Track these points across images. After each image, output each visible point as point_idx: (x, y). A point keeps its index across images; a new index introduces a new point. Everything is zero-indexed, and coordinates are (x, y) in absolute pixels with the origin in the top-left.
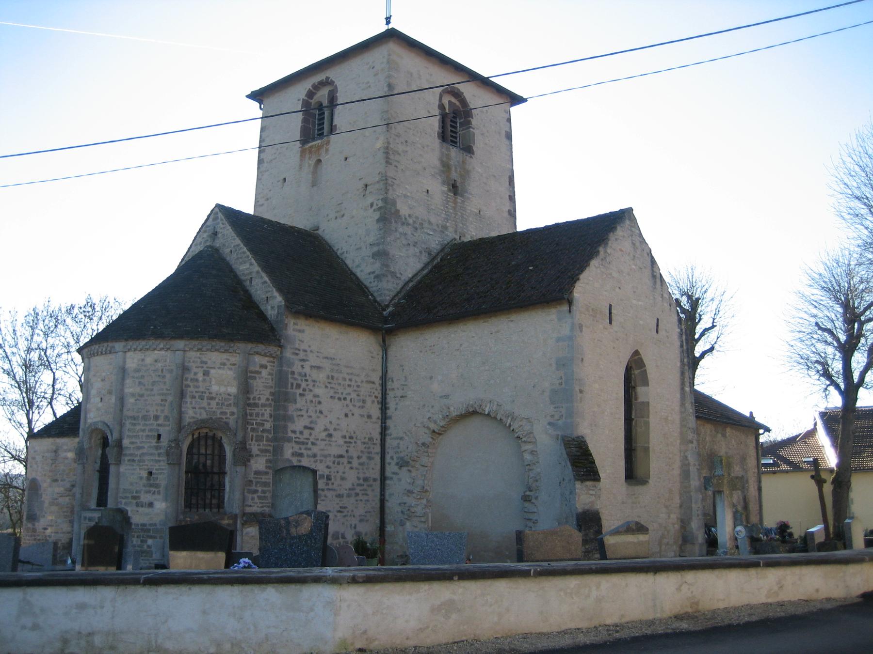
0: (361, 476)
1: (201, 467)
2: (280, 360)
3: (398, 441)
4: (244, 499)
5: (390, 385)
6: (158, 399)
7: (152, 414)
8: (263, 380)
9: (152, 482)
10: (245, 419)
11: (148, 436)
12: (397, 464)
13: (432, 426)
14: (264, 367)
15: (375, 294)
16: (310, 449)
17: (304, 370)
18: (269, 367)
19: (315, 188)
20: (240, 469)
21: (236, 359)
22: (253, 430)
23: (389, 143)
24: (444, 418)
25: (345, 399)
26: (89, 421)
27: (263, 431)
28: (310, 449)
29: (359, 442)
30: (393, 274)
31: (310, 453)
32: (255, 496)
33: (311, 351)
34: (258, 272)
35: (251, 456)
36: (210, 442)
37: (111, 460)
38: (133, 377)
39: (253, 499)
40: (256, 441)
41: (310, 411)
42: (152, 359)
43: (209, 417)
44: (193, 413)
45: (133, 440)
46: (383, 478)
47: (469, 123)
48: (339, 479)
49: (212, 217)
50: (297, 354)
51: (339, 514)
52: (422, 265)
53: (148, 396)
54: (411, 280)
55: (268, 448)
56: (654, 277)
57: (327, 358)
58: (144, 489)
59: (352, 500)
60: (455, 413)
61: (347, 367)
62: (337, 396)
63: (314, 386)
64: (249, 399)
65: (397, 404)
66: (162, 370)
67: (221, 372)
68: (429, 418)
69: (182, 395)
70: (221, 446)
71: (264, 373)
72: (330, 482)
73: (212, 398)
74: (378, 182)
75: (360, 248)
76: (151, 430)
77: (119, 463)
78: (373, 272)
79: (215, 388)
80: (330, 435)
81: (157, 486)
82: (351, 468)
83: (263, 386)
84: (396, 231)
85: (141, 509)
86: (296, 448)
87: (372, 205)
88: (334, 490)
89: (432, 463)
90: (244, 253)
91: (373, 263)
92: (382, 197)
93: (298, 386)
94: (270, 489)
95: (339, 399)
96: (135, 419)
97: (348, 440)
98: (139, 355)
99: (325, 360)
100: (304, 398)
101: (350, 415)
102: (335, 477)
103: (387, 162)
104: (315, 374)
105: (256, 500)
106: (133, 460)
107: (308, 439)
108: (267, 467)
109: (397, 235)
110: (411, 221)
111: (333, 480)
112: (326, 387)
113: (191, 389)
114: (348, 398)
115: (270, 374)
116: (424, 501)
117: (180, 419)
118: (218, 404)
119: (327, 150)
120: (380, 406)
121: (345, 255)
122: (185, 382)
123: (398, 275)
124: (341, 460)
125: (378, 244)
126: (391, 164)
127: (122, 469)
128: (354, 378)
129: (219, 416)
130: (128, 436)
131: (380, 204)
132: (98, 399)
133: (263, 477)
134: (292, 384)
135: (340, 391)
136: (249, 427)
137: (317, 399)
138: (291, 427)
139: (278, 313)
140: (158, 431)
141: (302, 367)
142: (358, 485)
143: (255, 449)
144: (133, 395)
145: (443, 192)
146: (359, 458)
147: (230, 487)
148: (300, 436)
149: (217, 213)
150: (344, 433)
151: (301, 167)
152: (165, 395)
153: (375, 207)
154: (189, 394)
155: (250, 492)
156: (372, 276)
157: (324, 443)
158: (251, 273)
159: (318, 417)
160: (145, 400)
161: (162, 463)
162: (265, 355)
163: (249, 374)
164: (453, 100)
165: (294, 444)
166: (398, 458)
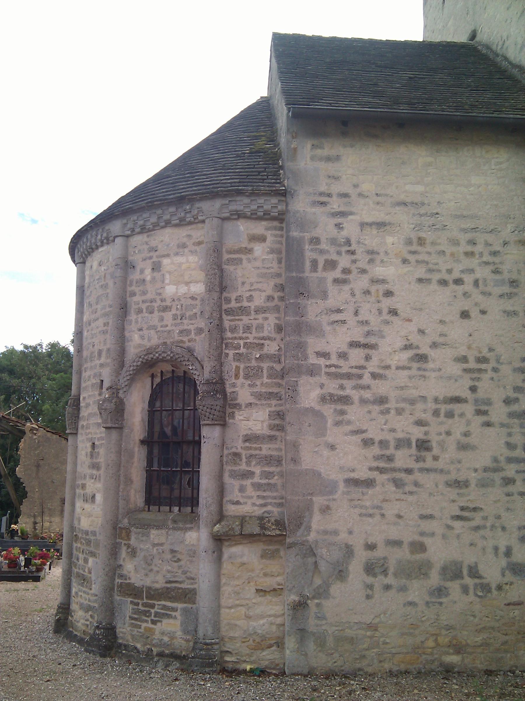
14: (262, 239)
17: (344, 233)
18: (270, 239)
21: (198, 233)
22: (238, 357)
25: (458, 282)
27: (261, 359)
28: (368, 387)
29: (506, 370)
32: (248, 483)
33: (360, 195)
37: (260, 456)
39: (242, 489)
51: (457, 524)
59: (496, 492)
62: (436, 277)
67: (179, 259)
69: (124, 309)
71: (259, 249)
72: (429, 456)
73: (166, 309)
79: (170, 290)
80: (422, 358)
82: (488, 424)
86: (332, 387)
97: (472, 364)
100: (346, 288)
101: (474, 313)
102: (442, 444)
105: (250, 491)
108: (272, 427)
111: (436, 451)
112: (405, 261)
113: (137, 298)
114: (468, 279)
115: (272, 251)
122: (129, 289)
124: (457, 408)
128: (481, 238)
129: (177, 338)
133: (264, 447)
134: (314, 263)
136: (231, 353)
137: (382, 288)
141: (338, 226)
142: (510, 460)
143: (242, 391)
148: (341, 363)
150: (462, 351)
155: (234, 475)
157: (406, 373)
162: (254, 217)
165: (324, 379)
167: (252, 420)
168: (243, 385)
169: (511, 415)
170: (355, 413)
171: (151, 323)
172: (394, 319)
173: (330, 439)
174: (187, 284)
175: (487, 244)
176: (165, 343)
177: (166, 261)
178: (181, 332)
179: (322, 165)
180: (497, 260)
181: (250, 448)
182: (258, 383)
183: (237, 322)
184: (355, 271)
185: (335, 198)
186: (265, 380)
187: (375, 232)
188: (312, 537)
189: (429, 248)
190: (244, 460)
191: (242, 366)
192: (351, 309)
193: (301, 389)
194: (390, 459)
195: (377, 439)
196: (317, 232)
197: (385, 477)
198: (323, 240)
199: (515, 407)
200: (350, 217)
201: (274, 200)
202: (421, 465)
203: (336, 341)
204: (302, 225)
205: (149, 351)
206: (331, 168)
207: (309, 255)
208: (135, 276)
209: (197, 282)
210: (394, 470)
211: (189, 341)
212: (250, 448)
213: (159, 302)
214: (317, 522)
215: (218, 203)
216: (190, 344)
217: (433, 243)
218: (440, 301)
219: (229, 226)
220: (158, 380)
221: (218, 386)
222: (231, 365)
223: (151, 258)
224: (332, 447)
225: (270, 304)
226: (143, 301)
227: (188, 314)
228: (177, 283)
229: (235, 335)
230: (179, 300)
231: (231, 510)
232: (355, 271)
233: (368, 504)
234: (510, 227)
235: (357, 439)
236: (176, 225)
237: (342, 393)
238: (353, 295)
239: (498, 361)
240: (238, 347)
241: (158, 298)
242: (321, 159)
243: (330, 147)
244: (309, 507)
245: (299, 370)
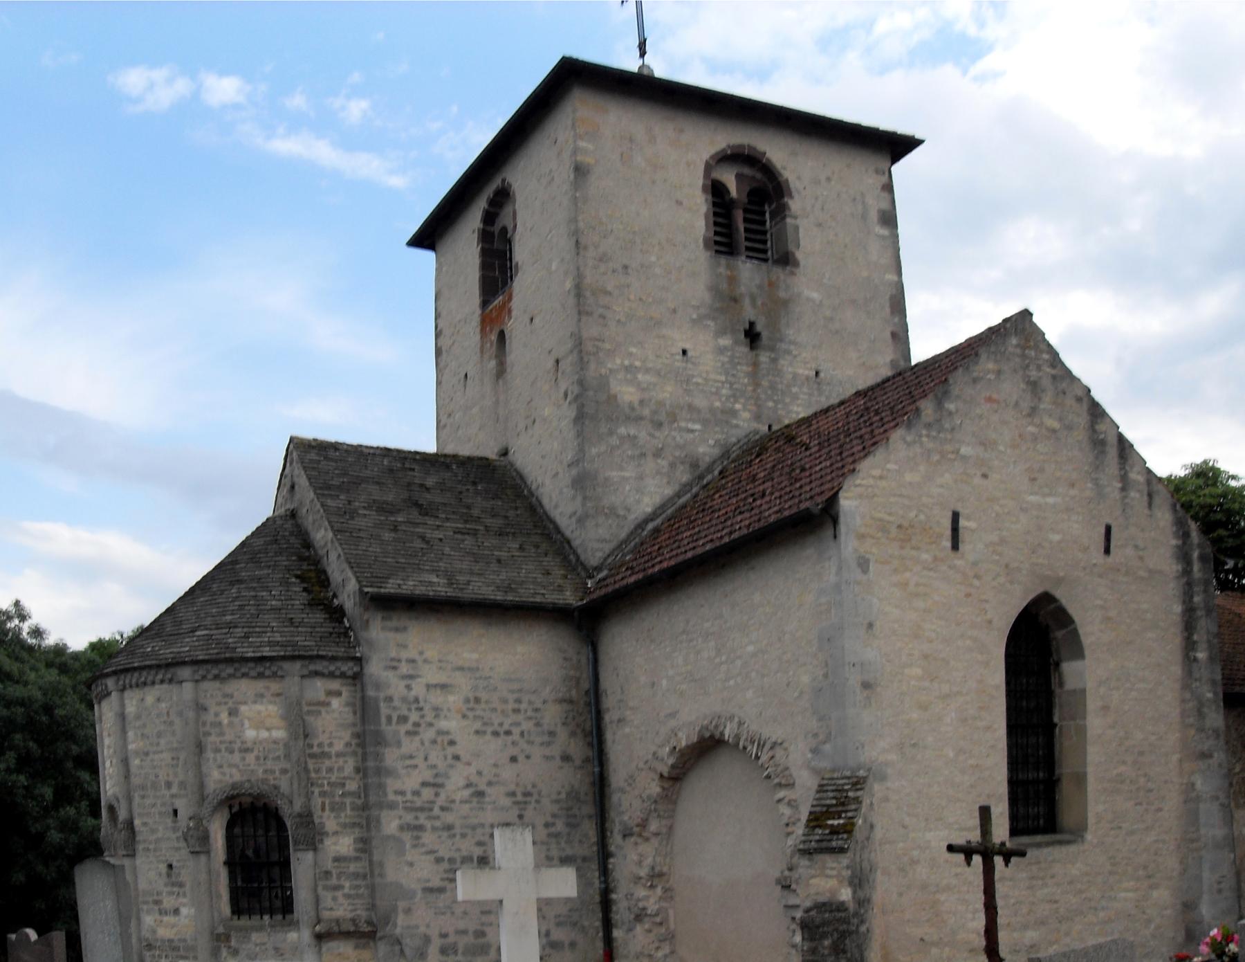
4: (317, 901)
6: (167, 756)
7: (162, 778)
9: (174, 879)
10: (307, 781)
11: (160, 813)
14: (339, 694)
16: (438, 818)
17: (413, 693)
21: (275, 686)
25: (508, 733)
28: (438, 818)
29: (546, 801)
30: (612, 512)
31: (438, 824)
32: (339, 894)
33: (425, 661)
36: (260, 816)
39: (334, 899)
40: (332, 810)
41: (430, 757)
43: (245, 778)
44: (222, 774)
45: (145, 820)
52: (677, 487)
53: (155, 753)
54: (647, 521)
56: (1098, 444)
57: (461, 669)
58: (166, 889)
62: (490, 730)
67: (258, 707)
69: (200, 748)
71: (335, 703)
73: (247, 750)
79: (250, 734)
80: (480, 794)
81: (181, 885)
85: (166, 919)
86: (409, 818)
89: (671, 828)
93: (403, 719)
97: (520, 798)
99: (458, 673)
100: (417, 739)
101: (521, 758)
104: (436, 698)
105: (341, 900)
106: (148, 850)
107: (433, 802)
108: (357, 850)
109: (614, 441)
110: (646, 412)
112: (464, 716)
113: (212, 738)
115: (347, 704)
116: (659, 891)
117: (202, 786)
118: (258, 758)
123: (622, 513)
127: (138, 862)
130: (139, 815)
134: (389, 718)
136: (317, 791)
138: (392, 784)
140: (173, 804)
141: (408, 687)
143: (330, 822)
144: (137, 753)
145: (721, 351)
148: (416, 798)
150: (512, 787)
154: (209, 747)
155: (326, 888)
156: (574, 519)
157: (467, 806)
159: (451, 766)
162: (331, 675)
164: (747, 171)
165: (401, 812)
167: (341, 844)
168: (329, 817)
169: (549, 835)
170: (428, 838)
172: (458, 764)
173: (409, 858)
174: (268, 729)
175: (530, 703)
176: (249, 781)
177: (243, 708)
178: (265, 771)
179: (391, 635)
180: (538, 715)
185: (403, 663)
187: (439, 691)
188: (398, 931)
189: (483, 706)
192: (422, 756)
193: (383, 821)
195: (447, 857)
196: (391, 692)
198: (396, 698)
199: (552, 830)
200: (419, 680)
201: (351, 664)
203: (410, 782)
204: (378, 686)
205: (234, 786)
206: (400, 637)
207: (384, 710)
208: (209, 717)
214: (401, 920)
217: (487, 702)
218: (492, 748)
219: (307, 682)
220: (235, 809)
221: (306, 818)
222: (317, 801)
223: (226, 703)
224: (411, 864)
228: (257, 728)
230: (261, 742)
231: (326, 915)
233: (441, 905)
234: (548, 689)
235: (431, 857)
236: (254, 678)
238: (422, 743)
239: (539, 794)
242: (390, 630)
244: (394, 909)
245: (381, 806)
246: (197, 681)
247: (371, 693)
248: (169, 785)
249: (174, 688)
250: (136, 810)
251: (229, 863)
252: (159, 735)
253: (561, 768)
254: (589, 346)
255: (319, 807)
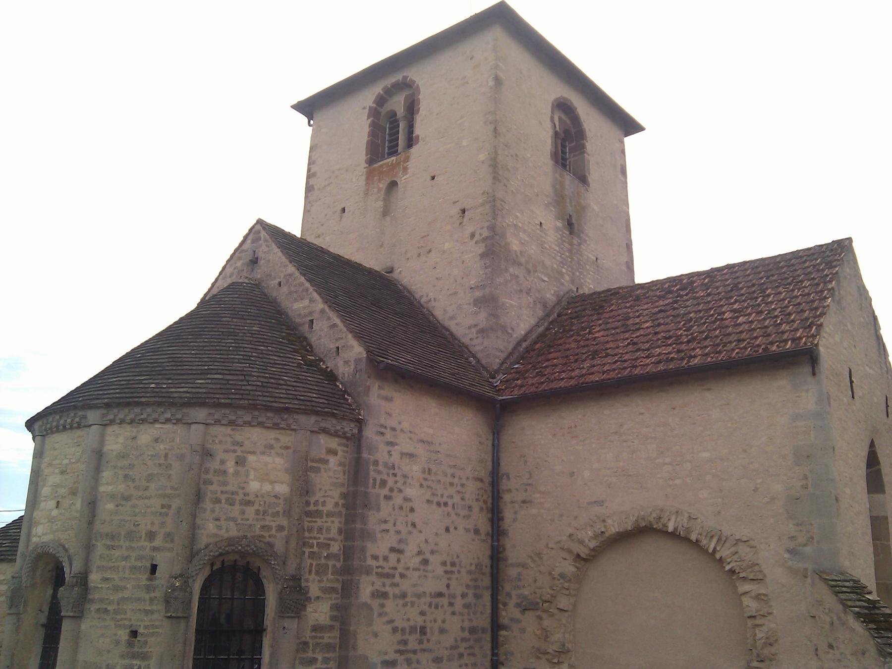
0: (466, 624)
1: (222, 620)
2: (356, 441)
3: (520, 570)
5: (504, 484)
8: (331, 474)
9: (136, 649)
11: (133, 568)
12: (518, 605)
13: (577, 549)
14: (334, 452)
15: (479, 355)
16: (397, 585)
17: (392, 459)
18: (340, 453)
19: (388, 218)
20: (291, 625)
21: (286, 439)
22: (312, 555)
23: (496, 152)
24: (596, 537)
26: (34, 540)
28: (397, 585)
30: (503, 328)
34: (323, 311)
35: (308, 599)
36: (239, 576)
38: (115, 467)
40: (317, 573)
41: (398, 523)
42: (147, 443)
43: (241, 534)
44: (216, 528)
45: (108, 575)
46: (496, 626)
47: (583, 147)
48: (436, 632)
49: (250, 237)
50: (382, 434)
54: (524, 339)
55: (335, 585)
60: (614, 527)
61: (449, 456)
62: (436, 499)
63: (405, 483)
64: (308, 503)
65: (516, 513)
66: (166, 456)
67: (266, 458)
68: (570, 536)
69: (198, 497)
70: (260, 588)
71: (333, 461)
72: (425, 638)
73: (249, 503)
74: (482, 205)
75: (455, 293)
76: (140, 558)
77: (79, 617)
78: (476, 325)
79: (254, 486)
81: (145, 657)
82: (454, 613)
83: (329, 483)
84: (506, 270)
87: (473, 236)
88: (430, 651)
89: (574, 605)
90: (301, 284)
91: (476, 313)
92: (487, 224)
93: (384, 483)
94: (336, 655)
95: (439, 504)
96: (113, 537)
97: (449, 568)
98: (127, 431)
100: (391, 503)
101: (452, 529)
102: (431, 628)
103: (494, 178)
106: (106, 611)
107: (395, 569)
108: (333, 618)
110: (523, 260)
115: (341, 464)
117: (193, 539)
118: (257, 512)
119: (405, 169)
120: (490, 515)
121: (433, 303)
125: (483, 287)
126: (499, 181)
127: (84, 626)
129: (258, 532)
130: (101, 568)
131: (486, 233)
132: (52, 504)
133: (326, 635)
134: (375, 480)
135: (439, 492)
136: (307, 550)
137: (409, 505)
138: (372, 549)
139: (356, 371)
143: (314, 590)
144: (112, 496)
146: (463, 596)
147: (272, 655)
149: (259, 232)
151: (366, 194)
152: (168, 496)
153: (477, 237)
156: (474, 330)
157: (417, 573)
158: (311, 313)
159: (410, 533)
160: (134, 506)
161: (155, 616)
162: (335, 434)
163: (310, 464)
165: (373, 578)
166: (518, 596)
167: (319, 612)
170: (390, 606)
171: (231, 515)
173: (375, 628)
174: (272, 483)
177: (251, 458)
178: (263, 527)
181: (316, 637)
182: (325, 579)
183: (313, 524)
184: (396, 490)
186: (330, 577)
190: (311, 648)
191: (314, 564)
192: (392, 521)
194: (405, 643)
197: (403, 657)
198: (380, 463)
202: (421, 646)
205: (231, 541)
208: (214, 465)
209: (282, 483)
210: (407, 651)
211: (270, 536)
212: (316, 637)
213: (241, 496)
215: (313, 419)
216: (270, 540)
223: (235, 451)
225: (337, 510)
226: (222, 492)
227: (270, 511)
229: (311, 535)
230: (262, 496)
232: (396, 490)
235: (389, 627)
237: (383, 590)
240: (312, 547)
241: (241, 492)
243: (389, 391)
246: (105, 425)
247: (365, 455)
248: (151, 536)
249: (180, 430)
250: (96, 562)
251: (197, 631)
252: (150, 478)
253: (473, 540)
254: (498, 203)
255: (307, 570)
